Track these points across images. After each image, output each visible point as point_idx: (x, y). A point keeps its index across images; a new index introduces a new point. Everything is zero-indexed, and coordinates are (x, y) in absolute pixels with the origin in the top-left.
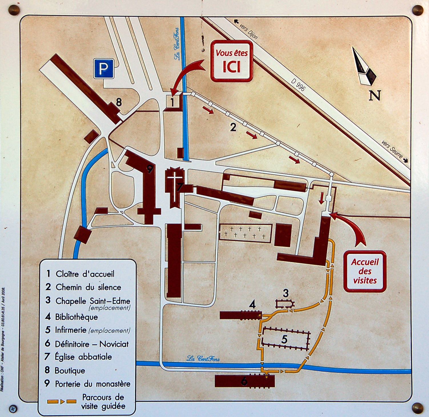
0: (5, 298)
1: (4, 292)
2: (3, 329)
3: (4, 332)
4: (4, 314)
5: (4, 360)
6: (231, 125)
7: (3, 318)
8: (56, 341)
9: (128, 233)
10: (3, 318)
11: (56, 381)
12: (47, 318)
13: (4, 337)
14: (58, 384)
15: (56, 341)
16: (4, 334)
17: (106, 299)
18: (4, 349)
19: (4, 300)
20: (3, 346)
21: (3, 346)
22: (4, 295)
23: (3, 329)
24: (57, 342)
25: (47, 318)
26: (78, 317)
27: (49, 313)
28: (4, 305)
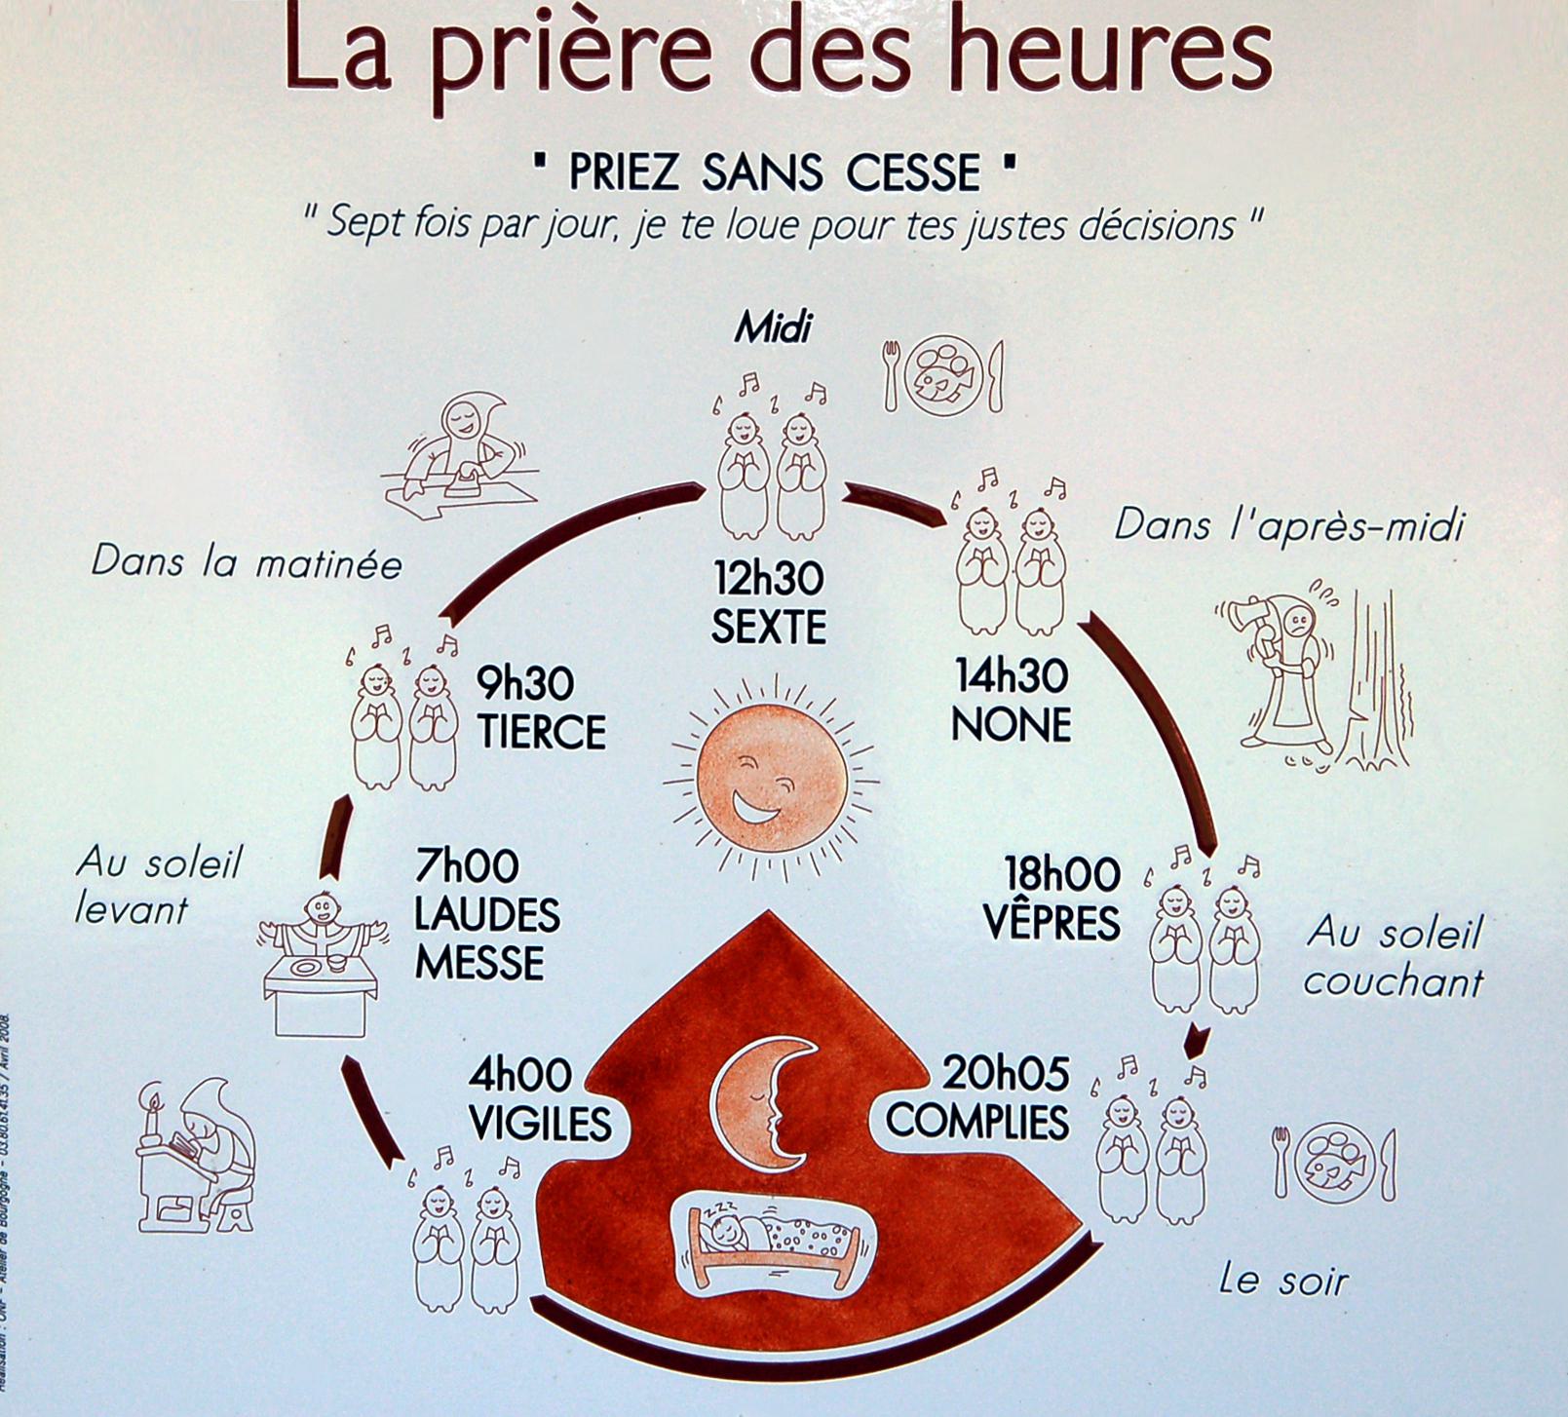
0: (9, 1051)
1: (8, 1029)
2: (2, 1164)
3: (8, 1177)
4: (7, 1109)
5: (7, 1276)
6: (947, 1063)
7: (4, 1124)
8: (440, 34)
9: (1351, 864)
10: (4, 1124)
11: (575, 156)
12: (475, 1080)
13: (6, 1194)
14: (551, 731)
15: (440, 34)
16: (8, 1184)
17: (1483, 975)
18: (7, 1239)
19: (6, 1060)
20: (6, 1226)
21: (6, 1226)
22: (7, 1040)
23: (2, 1164)
24: (497, 904)
25: (475, 1080)
26: (1007, 1076)
27: (421, 947)
28: (8, 1079)
